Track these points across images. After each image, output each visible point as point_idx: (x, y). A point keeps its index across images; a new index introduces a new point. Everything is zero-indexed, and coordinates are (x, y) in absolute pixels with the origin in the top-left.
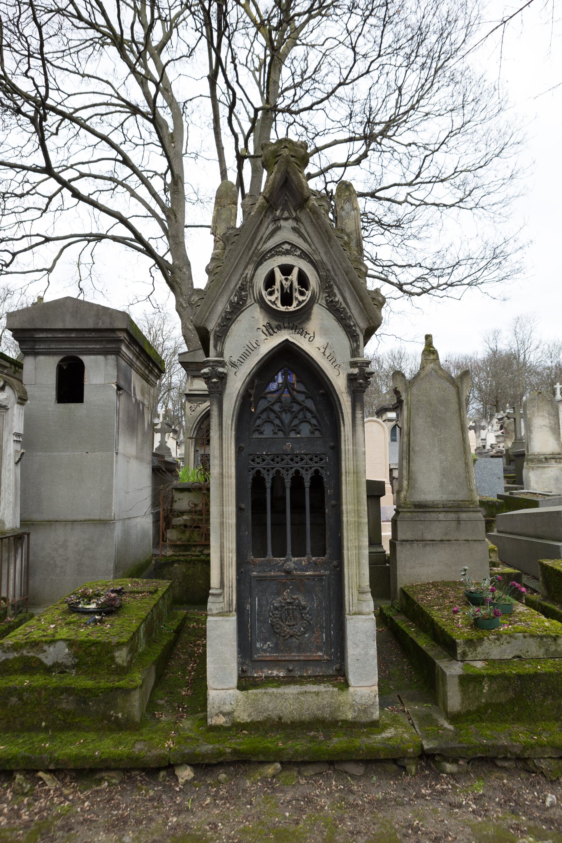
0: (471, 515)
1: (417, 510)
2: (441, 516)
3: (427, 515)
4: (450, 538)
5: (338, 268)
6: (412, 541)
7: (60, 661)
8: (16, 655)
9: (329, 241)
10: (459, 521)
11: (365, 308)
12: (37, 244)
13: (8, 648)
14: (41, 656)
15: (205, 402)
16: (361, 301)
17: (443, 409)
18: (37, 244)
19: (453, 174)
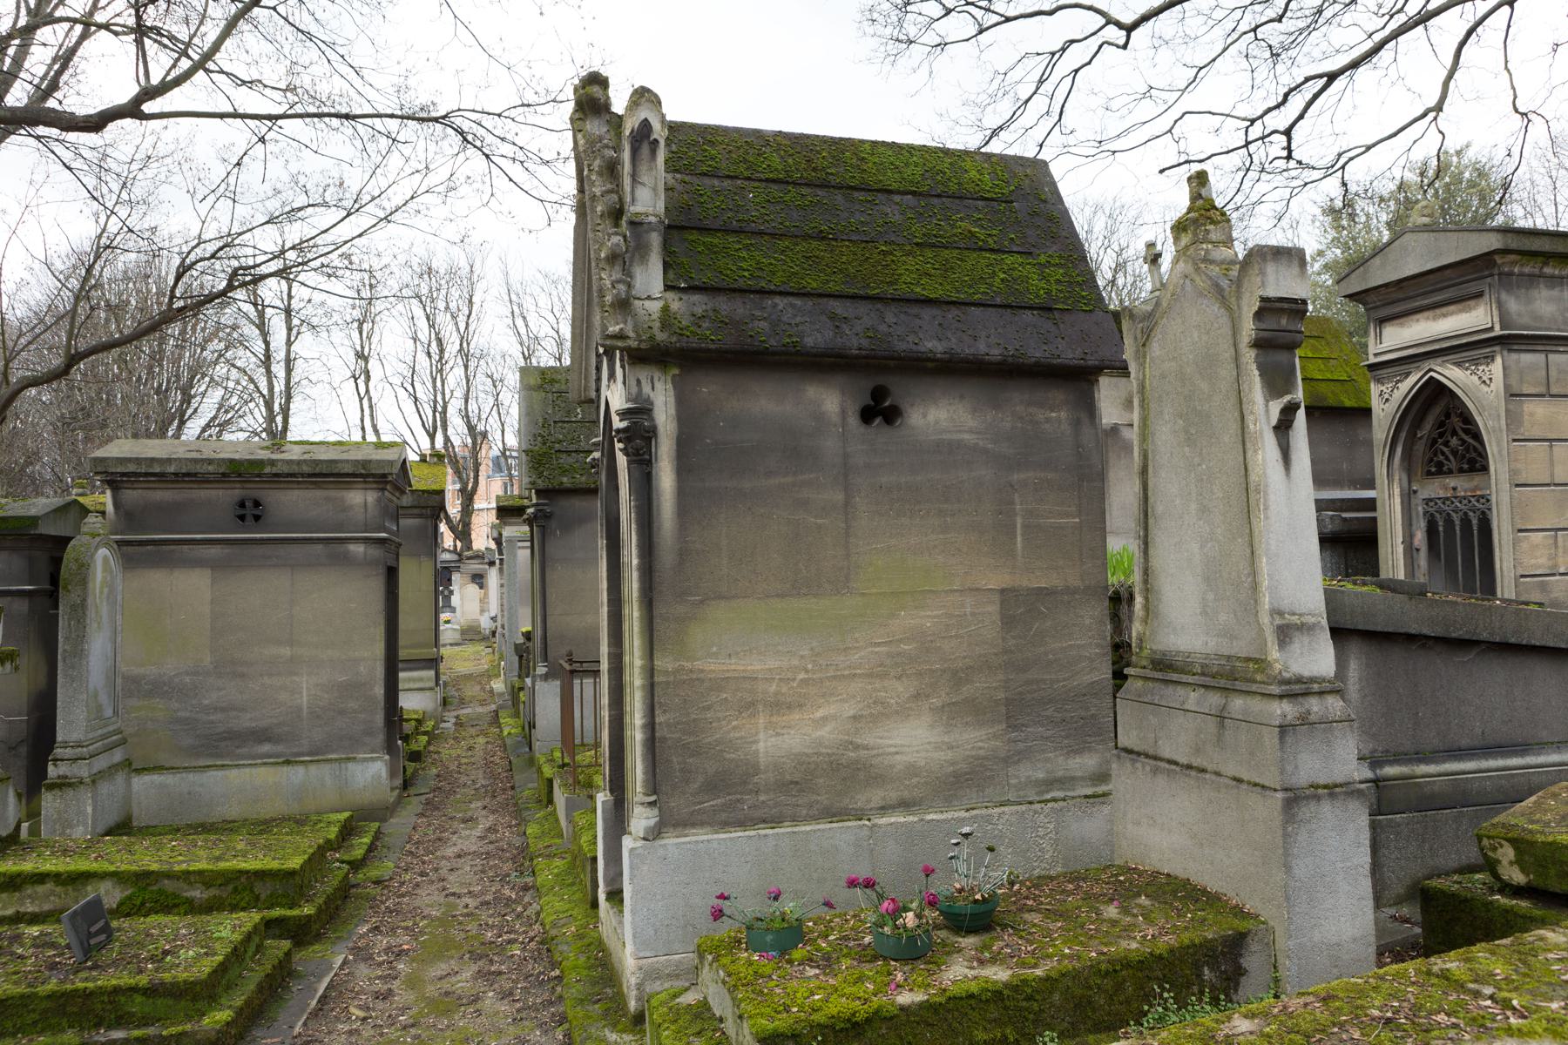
0: (1256, 704)
1: (1159, 675)
2: (1193, 698)
3: (1170, 689)
4: (1205, 764)
6: (1139, 754)
10: (1221, 717)
12: (1316, 96)
15: (1408, 375)
17: (1204, 386)
18: (1316, 96)
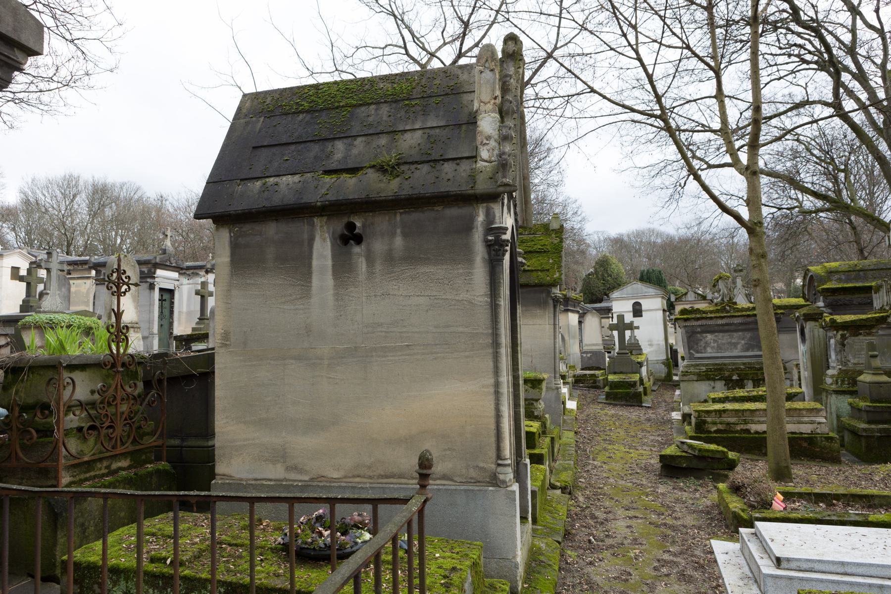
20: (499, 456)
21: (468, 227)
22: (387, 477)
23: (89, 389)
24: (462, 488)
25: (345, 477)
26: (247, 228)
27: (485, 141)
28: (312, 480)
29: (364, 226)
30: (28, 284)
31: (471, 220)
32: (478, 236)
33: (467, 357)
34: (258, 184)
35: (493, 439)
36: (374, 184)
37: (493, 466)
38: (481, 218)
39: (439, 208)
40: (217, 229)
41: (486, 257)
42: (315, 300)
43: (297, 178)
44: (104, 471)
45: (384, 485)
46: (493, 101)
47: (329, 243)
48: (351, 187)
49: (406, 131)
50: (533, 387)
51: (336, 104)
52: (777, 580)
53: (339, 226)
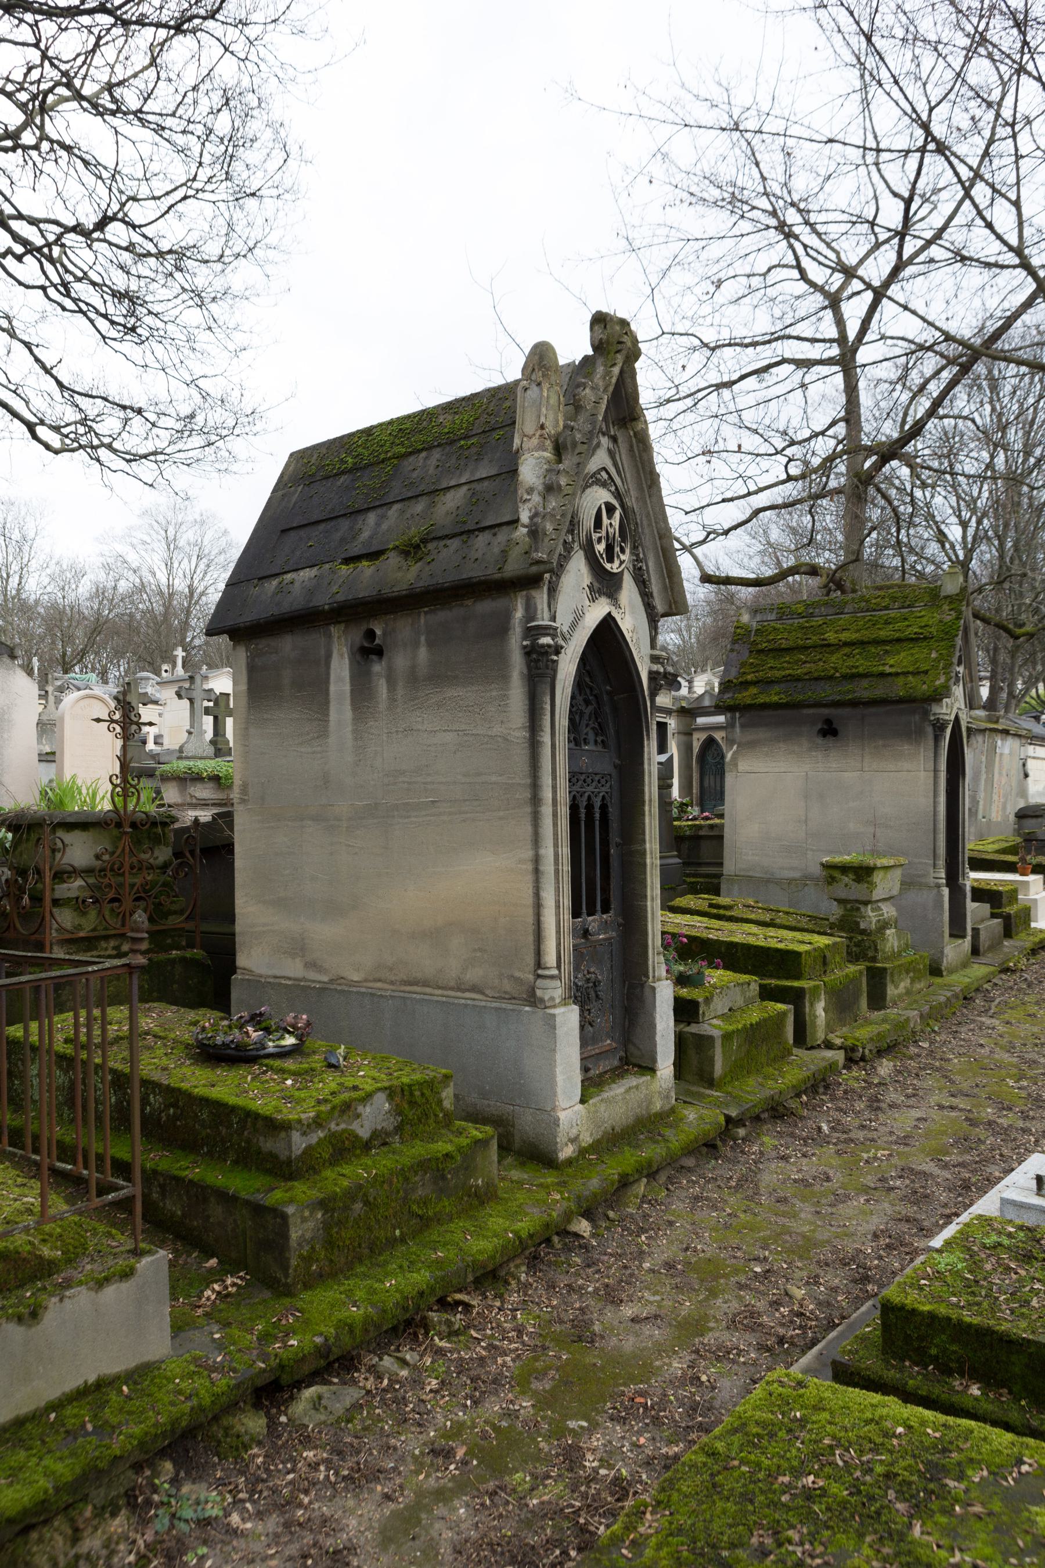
5: (650, 525)
7: (379, 1128)
8: (321, 1134)
9: (650, 487)
11: (672, 590)
13: (309, 1126)
14: (355, 1126)
16: (669, 577)
19: (84, 314)
20: (539, 964)
21: (503, 630)
22: (411, 984)
23: (92, 853)
24: (494, 1005)
25: (366, 980)
26: (263, 643)
27: (526, 497)
28: (331, 981)
29: (384, 634)
30: (216, 718)
31: (506, 616)
32: (516, 642)
33: (501, 818)
34: (275, 582)
35: (531, 938)
36: (400, 575)
37: (531, 977)
38: (519, 614)
39: (469, 602)
40: (234, 648)
41: (525, 671)
42: (332, 740)
43: (313, 572)
44: (110, 952)
45: (451, 1000)
46: (539, 432)
47: (347, 661)
48: (366, 580)
49: (449, 488)
50: (859, 880)
51: (382, 456)
52: (1023, 1211)
53: (357, 636)
